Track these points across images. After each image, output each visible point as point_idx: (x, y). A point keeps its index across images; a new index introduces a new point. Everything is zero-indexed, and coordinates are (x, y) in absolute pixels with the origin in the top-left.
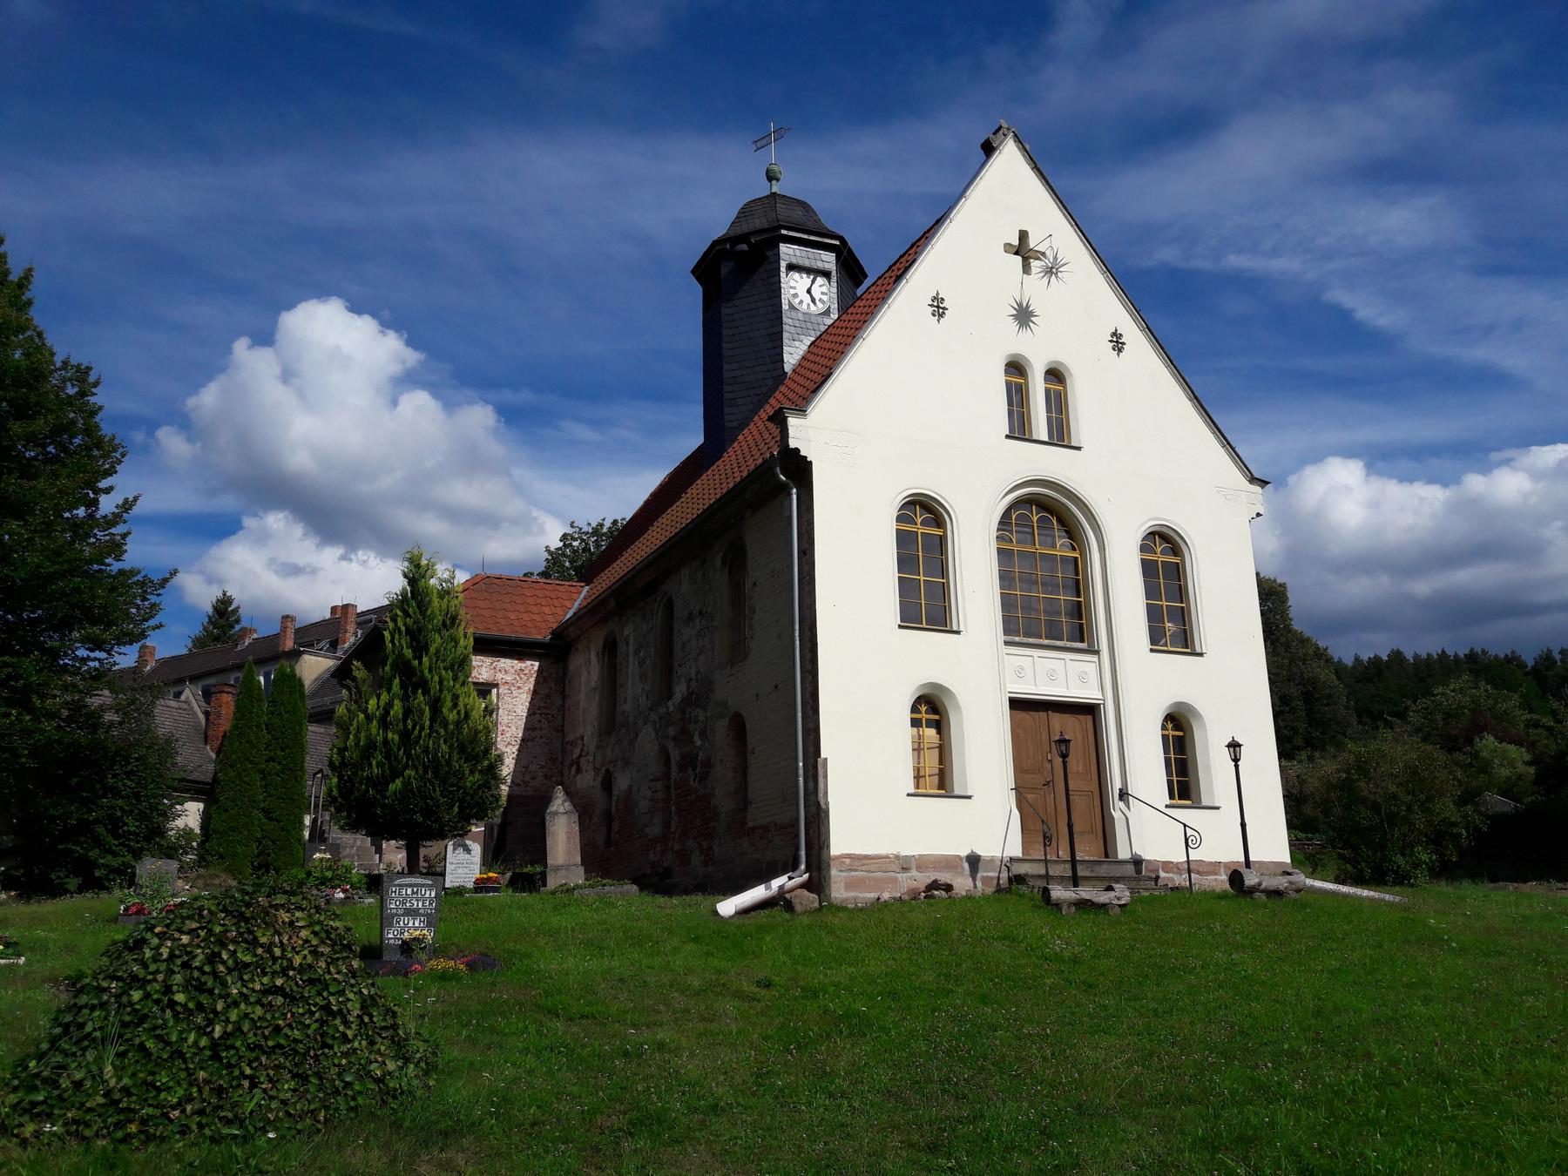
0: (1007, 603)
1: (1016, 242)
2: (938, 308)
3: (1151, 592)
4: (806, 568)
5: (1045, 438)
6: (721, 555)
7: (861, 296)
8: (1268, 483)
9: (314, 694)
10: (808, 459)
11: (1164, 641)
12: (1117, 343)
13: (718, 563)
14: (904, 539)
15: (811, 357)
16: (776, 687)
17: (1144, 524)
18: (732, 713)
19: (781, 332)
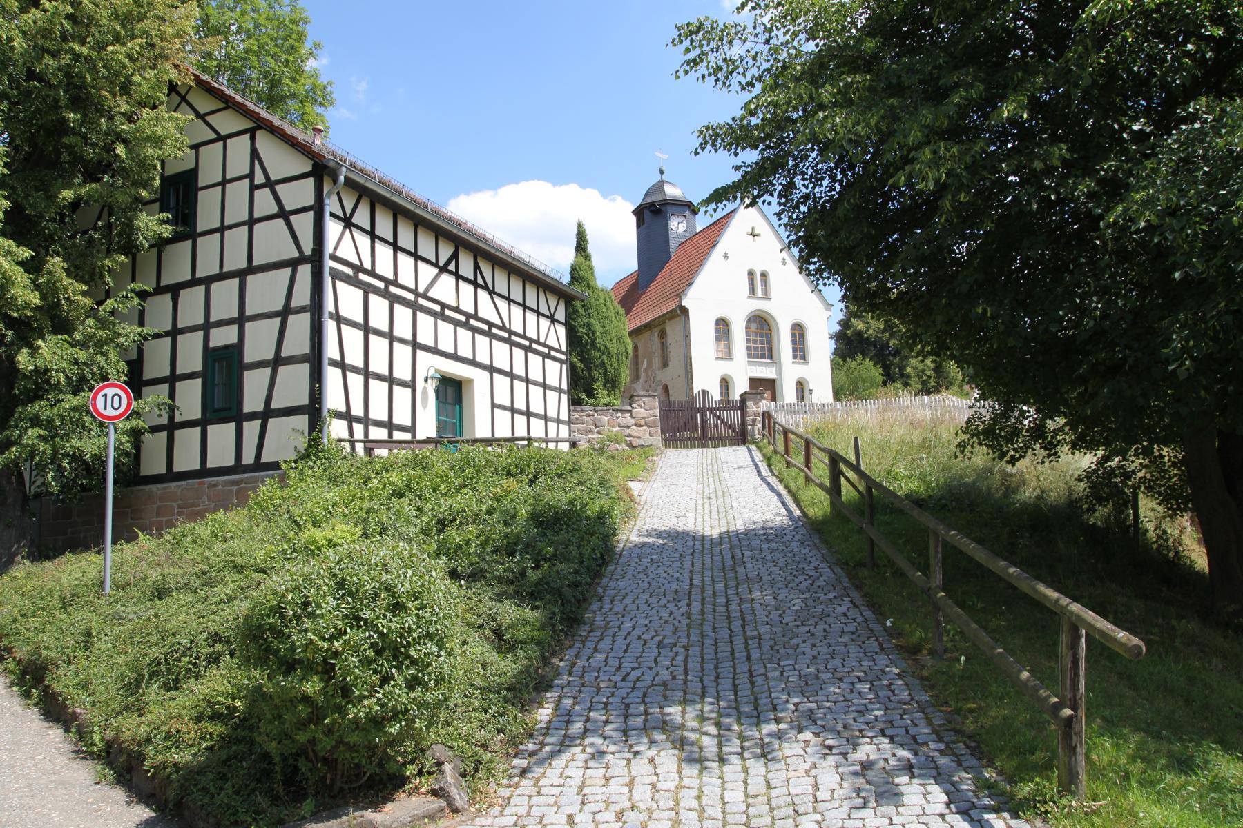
0: (749, 348)
2: (726, 257)
3: (794, 342)
5: (212, 345)
12: (784, 262)
14: (717, 331)
15: (707, 545)
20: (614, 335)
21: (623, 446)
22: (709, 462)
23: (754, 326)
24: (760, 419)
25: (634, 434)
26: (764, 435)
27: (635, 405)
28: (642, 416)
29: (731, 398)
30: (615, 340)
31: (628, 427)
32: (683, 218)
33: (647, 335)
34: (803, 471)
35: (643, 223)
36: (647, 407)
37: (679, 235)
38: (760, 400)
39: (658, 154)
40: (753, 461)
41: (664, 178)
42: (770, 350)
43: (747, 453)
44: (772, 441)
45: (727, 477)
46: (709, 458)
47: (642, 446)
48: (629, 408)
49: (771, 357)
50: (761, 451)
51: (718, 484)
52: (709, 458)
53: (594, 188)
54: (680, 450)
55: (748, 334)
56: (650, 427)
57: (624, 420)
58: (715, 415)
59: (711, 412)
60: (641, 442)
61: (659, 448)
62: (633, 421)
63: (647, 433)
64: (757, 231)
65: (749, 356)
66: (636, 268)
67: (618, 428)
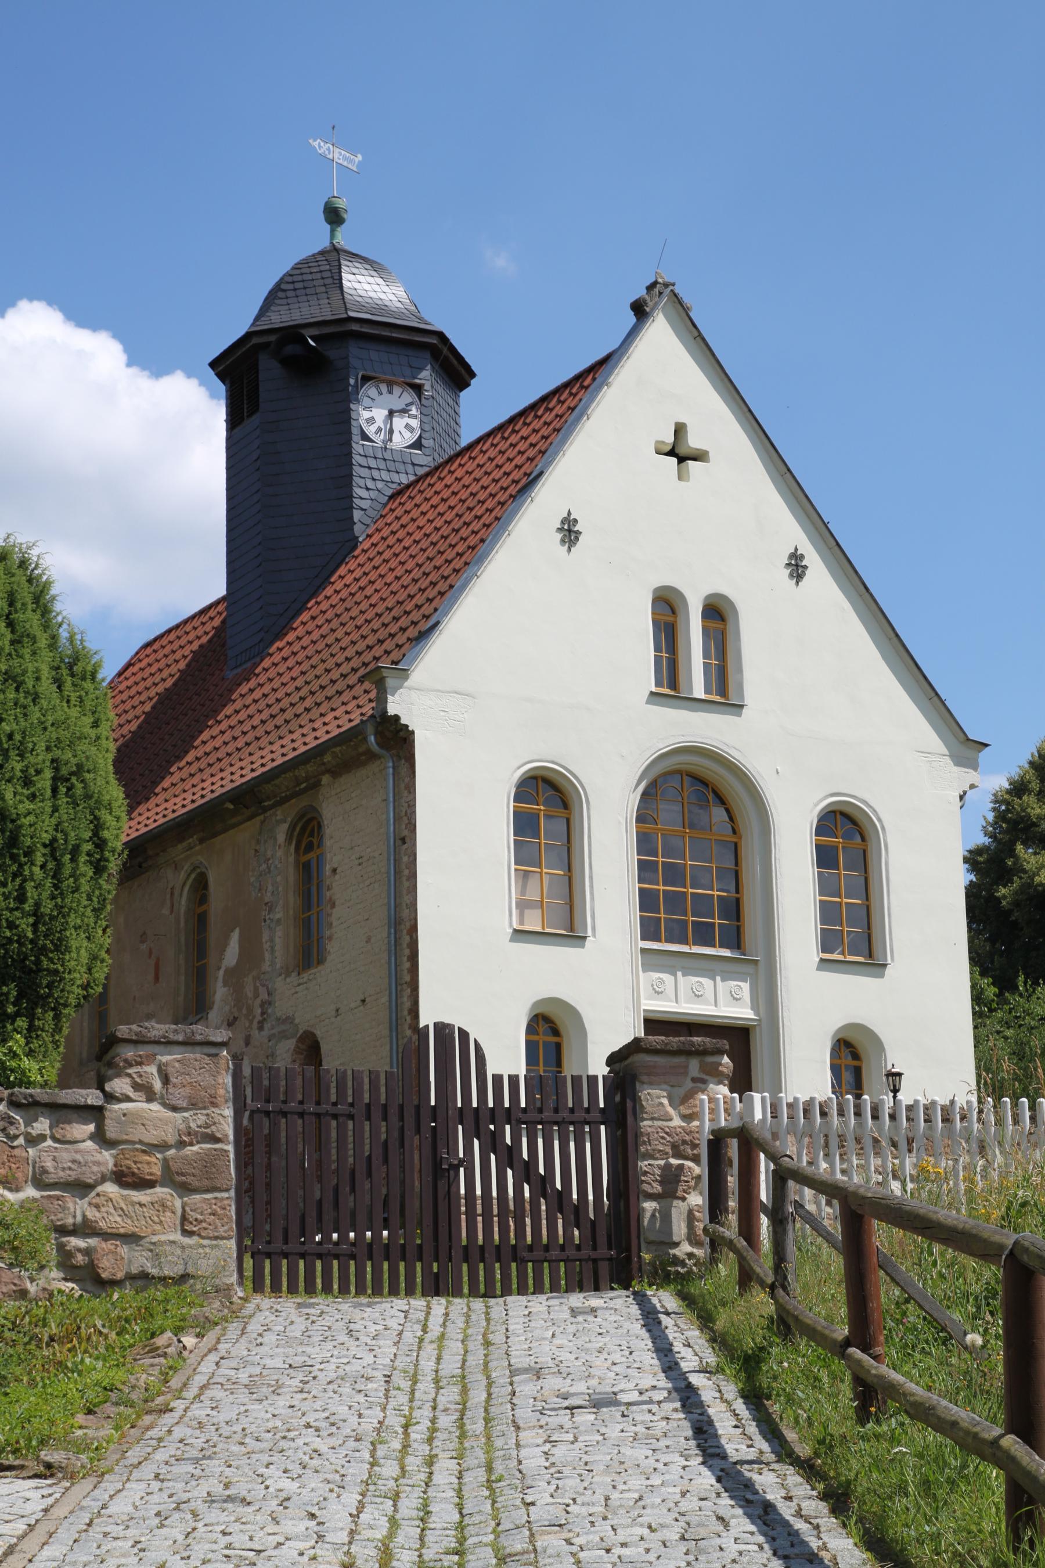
0: (647, 901)
1: (670, 439)
2: (569, 533)
4: (405, 859)
6: (285, 827)
7: (470, 447)
8: (986, 745)
9: (757, 1013)
10: (410, 729)
11: (840, 949)
12: (797, 568)
13: (281, 837)
16: (364, 1001)
17: (821, 800)
18: (301, 1032)
19: (350, 476)
20: (41, 757)
21: (54, 1279)
22: (451, 1365)
23: (669, 813)
24: (698, 1170)
25: (111, 1220)
26: (716, 1243)
27: (119, 1085)
28: (152, 1136)
29: (570, 1069)
30: (44, 782)
31: (81, 1188)
32: (408, 396)
33: (244, 834)
34: (992, 1452)
35: (254, 409)
36: (178, 1095)
37: (387, 457)
38: (701, 1084)
39: (321, 146)
40: (670, 1367)
41: (342, 239)
42: (734, 909)
43: (637, 1328)
44: (764, 1265)
45: (533, 1459)
46: (453, 1348)
47: (143, 1278)
48: (92, 1097)
49: (735, 939)
50: (705, 1320)
51: (477, 1501)
52: (453, 1348)
53: (117, 336)
54: (320, 1301)
55: (645, 843)
56: (184, 1189)
57: (66, 1155)
58: (493, 1143)
59: (475, 1130)
60: (139, 1260)
61: (224, 1291)
62: (107, 1158)
63: (171, 1219)
64: (694, 441)
65: (650, 930)
66: (220, 590)
67: (30, 1192)
